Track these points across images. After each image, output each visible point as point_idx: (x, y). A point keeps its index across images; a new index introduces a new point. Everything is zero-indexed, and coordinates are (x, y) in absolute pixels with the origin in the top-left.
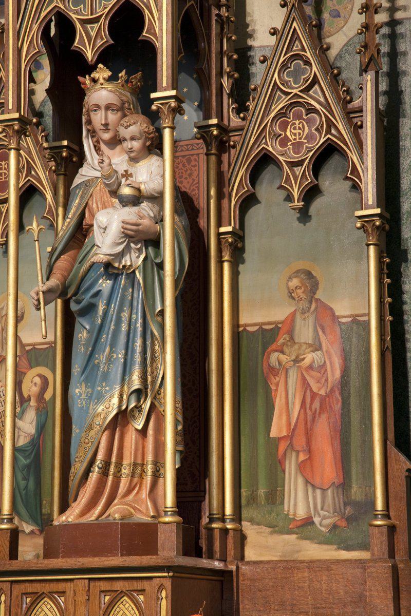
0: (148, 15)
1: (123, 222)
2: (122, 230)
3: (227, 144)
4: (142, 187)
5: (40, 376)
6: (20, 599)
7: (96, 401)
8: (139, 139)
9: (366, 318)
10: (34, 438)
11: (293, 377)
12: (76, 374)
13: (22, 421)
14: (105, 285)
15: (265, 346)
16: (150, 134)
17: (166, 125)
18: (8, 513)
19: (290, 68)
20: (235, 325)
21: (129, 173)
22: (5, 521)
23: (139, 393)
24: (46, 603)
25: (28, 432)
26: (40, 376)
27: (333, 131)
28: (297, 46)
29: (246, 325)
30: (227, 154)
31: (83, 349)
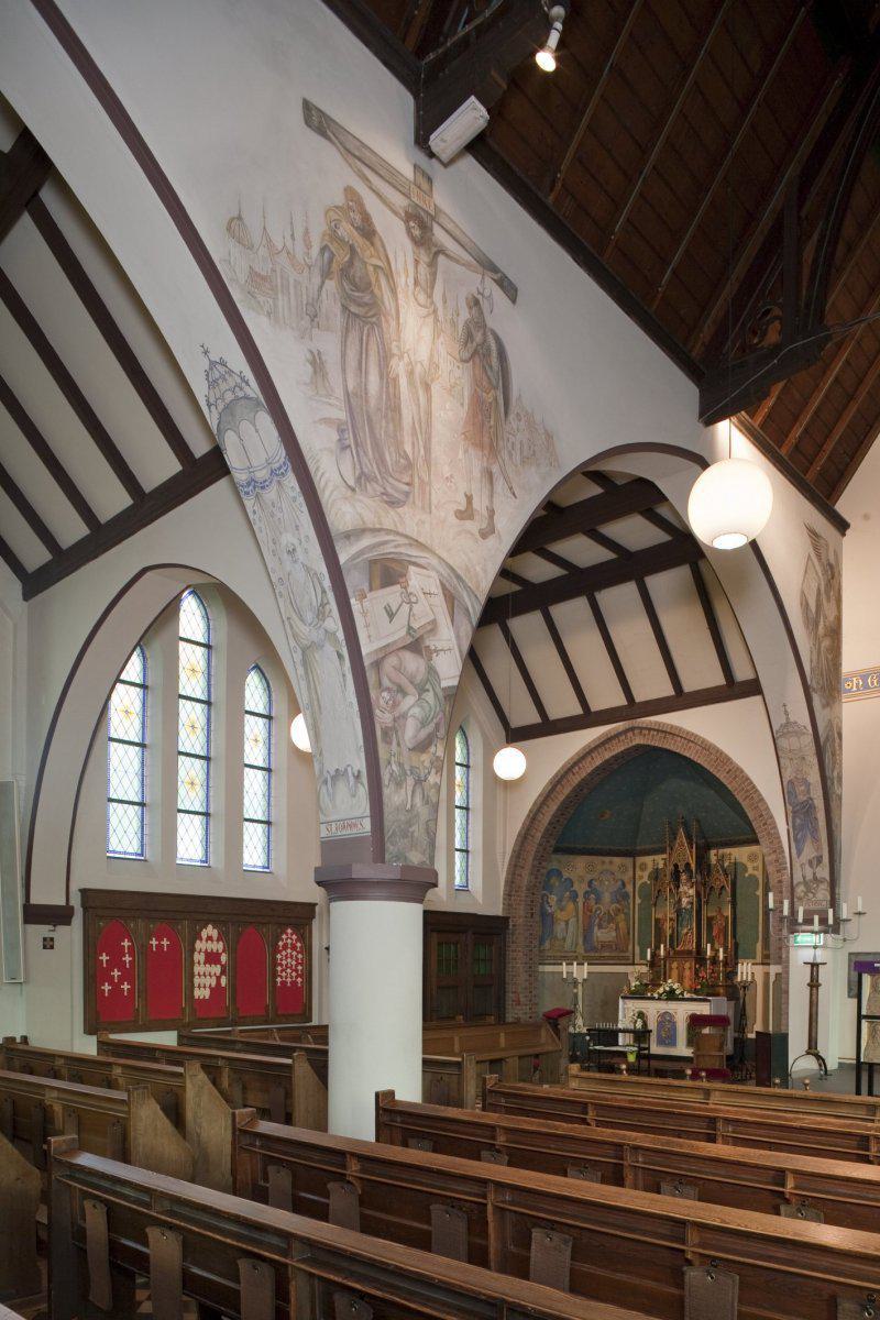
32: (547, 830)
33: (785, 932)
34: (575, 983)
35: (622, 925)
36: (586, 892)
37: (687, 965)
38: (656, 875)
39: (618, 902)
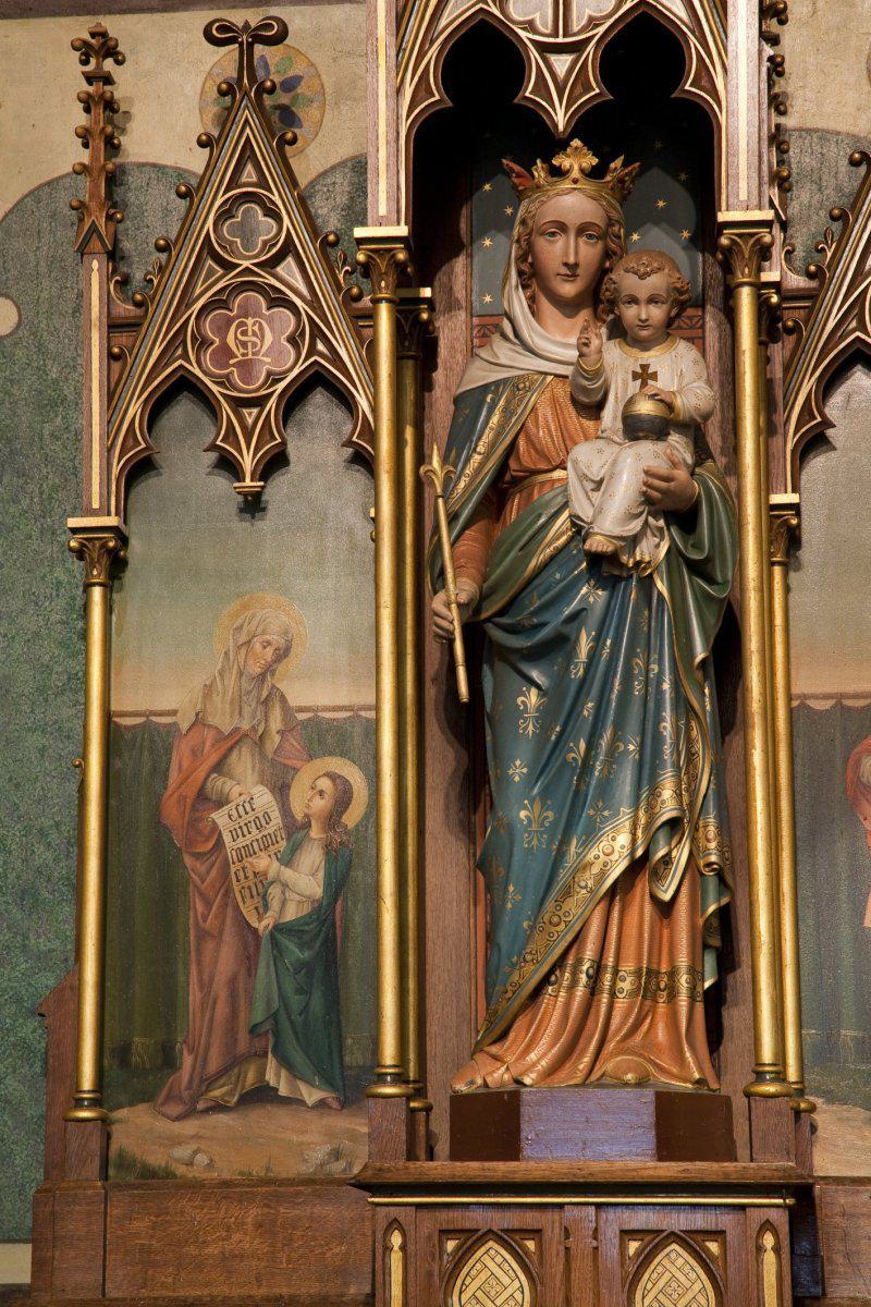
0: (696, 48)
1: (646, 473)
2: (644, 489)
3: (780, 325)
4: (678, 402)
5: (333, 777)
6: (436, 1242)
7: (584, 838)
8: (663, 303)
9: (371, 715)
10: (320, 906)
12: (517, 779)
13: (290, 867)
14: (591, 596)
16: (681, 293)
17: (745, 280)
18: (770, 1062)
19: (233, 217)
20: (108, 716)
21: (639, 370)
22: (389, 1078)
24: (492, 1252)
25: (308, 893)
26: (333, 777)
27: (320, 346)
28: (249, 176)
29: (805, 697)
30: (780, 344)
31: (531, 728)
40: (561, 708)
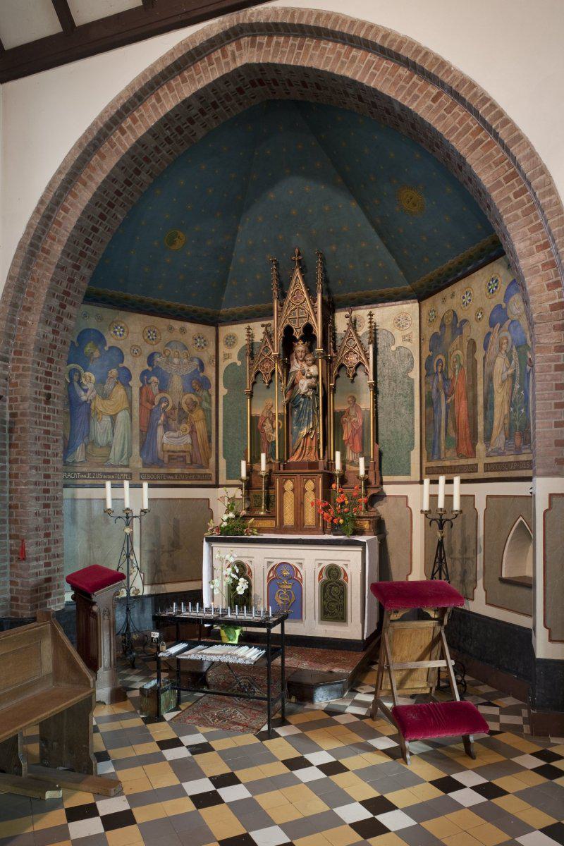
11: (349, 424)
14: (302, 400)
15: (342, 416)
20: (334, 410)
23: (312, 429)
32: (72, 240)
33: (89, 555)
34: (128, 517)
35: (200, 426)
36: (144, 373)
37: (310, 485)
38: (251, 351)
39: (194, 391)
40: (299, 414)
